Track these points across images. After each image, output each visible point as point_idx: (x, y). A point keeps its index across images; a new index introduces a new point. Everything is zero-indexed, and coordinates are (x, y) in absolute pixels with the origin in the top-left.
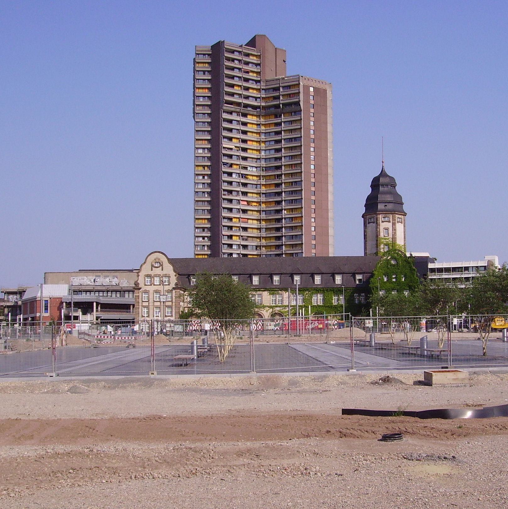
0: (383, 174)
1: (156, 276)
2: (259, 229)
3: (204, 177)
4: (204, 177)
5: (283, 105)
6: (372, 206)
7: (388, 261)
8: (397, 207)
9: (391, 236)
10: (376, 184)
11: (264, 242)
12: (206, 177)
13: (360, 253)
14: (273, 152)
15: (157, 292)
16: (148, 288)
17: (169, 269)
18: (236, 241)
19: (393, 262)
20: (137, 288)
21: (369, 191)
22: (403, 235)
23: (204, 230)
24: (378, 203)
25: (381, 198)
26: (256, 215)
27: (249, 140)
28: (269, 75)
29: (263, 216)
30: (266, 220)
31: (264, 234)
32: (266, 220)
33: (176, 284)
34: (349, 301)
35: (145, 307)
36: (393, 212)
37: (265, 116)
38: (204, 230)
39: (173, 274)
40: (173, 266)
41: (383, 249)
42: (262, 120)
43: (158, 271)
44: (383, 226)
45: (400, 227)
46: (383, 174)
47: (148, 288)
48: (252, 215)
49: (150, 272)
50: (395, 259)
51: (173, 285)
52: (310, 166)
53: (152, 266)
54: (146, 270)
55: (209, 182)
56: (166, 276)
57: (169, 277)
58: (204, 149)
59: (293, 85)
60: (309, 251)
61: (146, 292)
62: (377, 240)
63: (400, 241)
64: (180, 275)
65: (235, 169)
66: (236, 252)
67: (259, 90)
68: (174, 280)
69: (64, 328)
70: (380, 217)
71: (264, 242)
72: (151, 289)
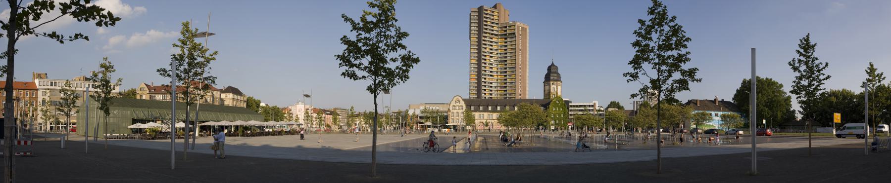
0: (553, 64)
6: (548, 79)
8: (558, 79)
10: (549, 68)
13: (857, 90)
17: (463, 103)
18: (487, 69)
20: (449, 110)
21: (546, 72)
22: (557, 89)
25: (552, 74)
27: (494, 47)
28: (502, 21)
36: (556, 80)
41: (552, 97)
44: (552, 86)
45: (559, 87)
46: (553, 64)
52: (519, 61)
54: (453, 103)
60: (518, 97)
63: (559, 94)
64: (467, 106)
65: (488, 50)
66: (488, 96)
68: (464, 108)
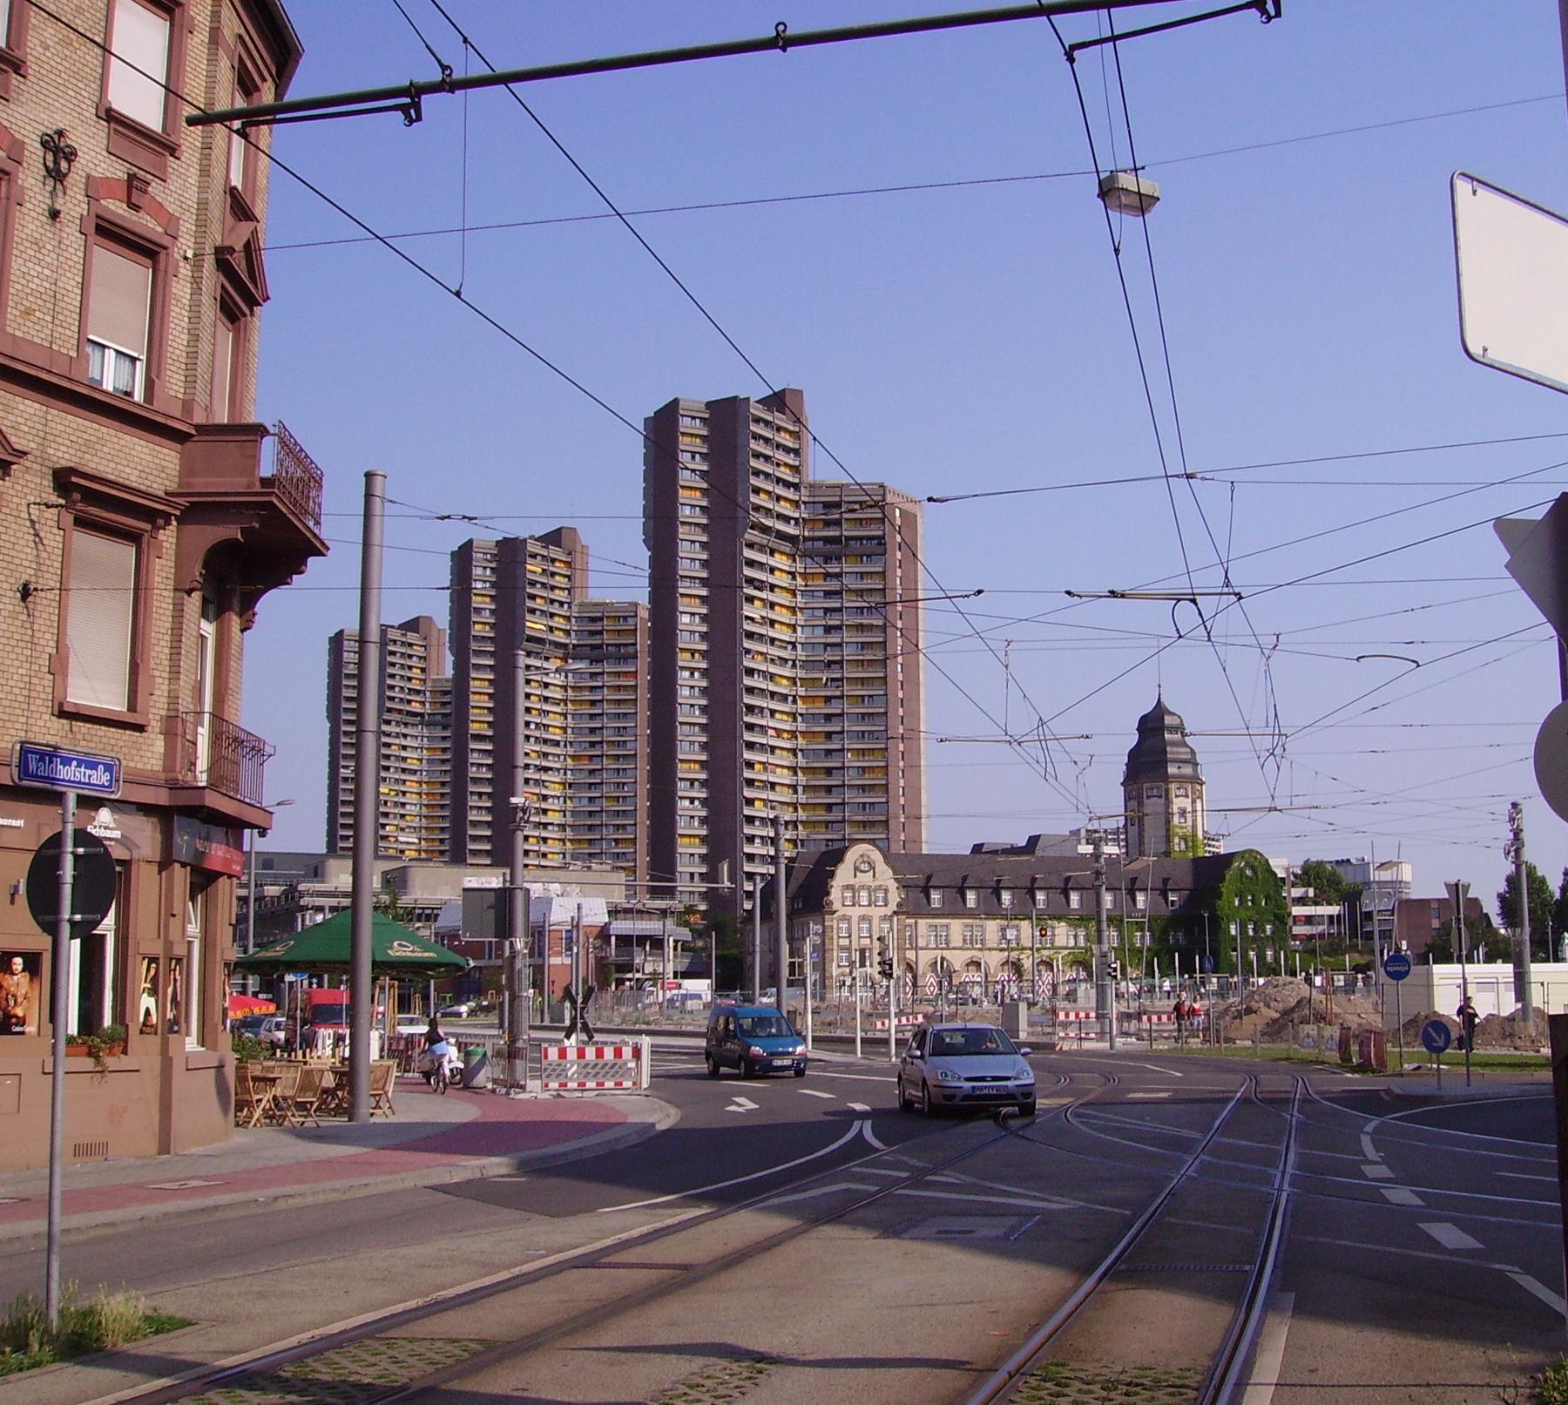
1: (863, 888)
2: (794, 788)
3: (692, 674)
4: (692, 674)
5: (856, 538)
7: (1242, 870)
9: (1189, 823)
11: (802, 815)
12: (697, 674)
14: (820, 631)
15: (863, 918)
16: (849, 911)
19: (1248, 872)
23: (692, 785)
24: (1166, 762)
26: (787, 760)
29: (801, 761)
30: (805, 770)
31: (802, 798)
32: (805, 770)
33: (899, 905)
34: (1160, 938)
35: (842, 949)
37: (806, 555)
38: (692, 785)
39: (892, 885)
40: (893, 868)
41: (1178, 845)
42: (800, 567)
43: (866, 878)
46: (1159, 710)
47: (849, 911)
48: (781, 758)
49: (852, 881)
50: (1253, 869)
51: (893, 907)
53: (856, 869)
55: (704, 684)
56: (879, 888)
57: (886, 891)
58: (693, 614)
59: (875, 502)
61: (845, 918)
62: (1168, 830)
64: (905, 886)
67: (796, 504)
68: (895, 898)
69: (252, 982)
70: (1173, 786)
71: (802, 815)
72: (854, 913)
